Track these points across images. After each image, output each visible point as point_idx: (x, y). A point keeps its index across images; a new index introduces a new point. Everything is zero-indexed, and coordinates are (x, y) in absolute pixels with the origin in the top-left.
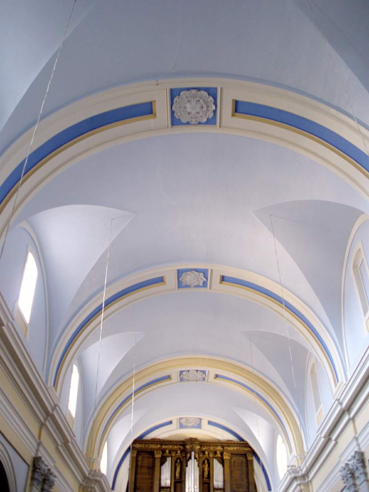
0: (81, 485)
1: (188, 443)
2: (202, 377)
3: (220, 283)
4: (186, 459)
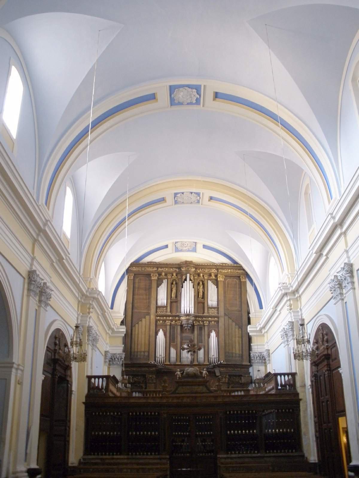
0: (79, 302)
1: (183, 266)
2: (196, 199)
3: (214, 100)
4: (181, 281)
